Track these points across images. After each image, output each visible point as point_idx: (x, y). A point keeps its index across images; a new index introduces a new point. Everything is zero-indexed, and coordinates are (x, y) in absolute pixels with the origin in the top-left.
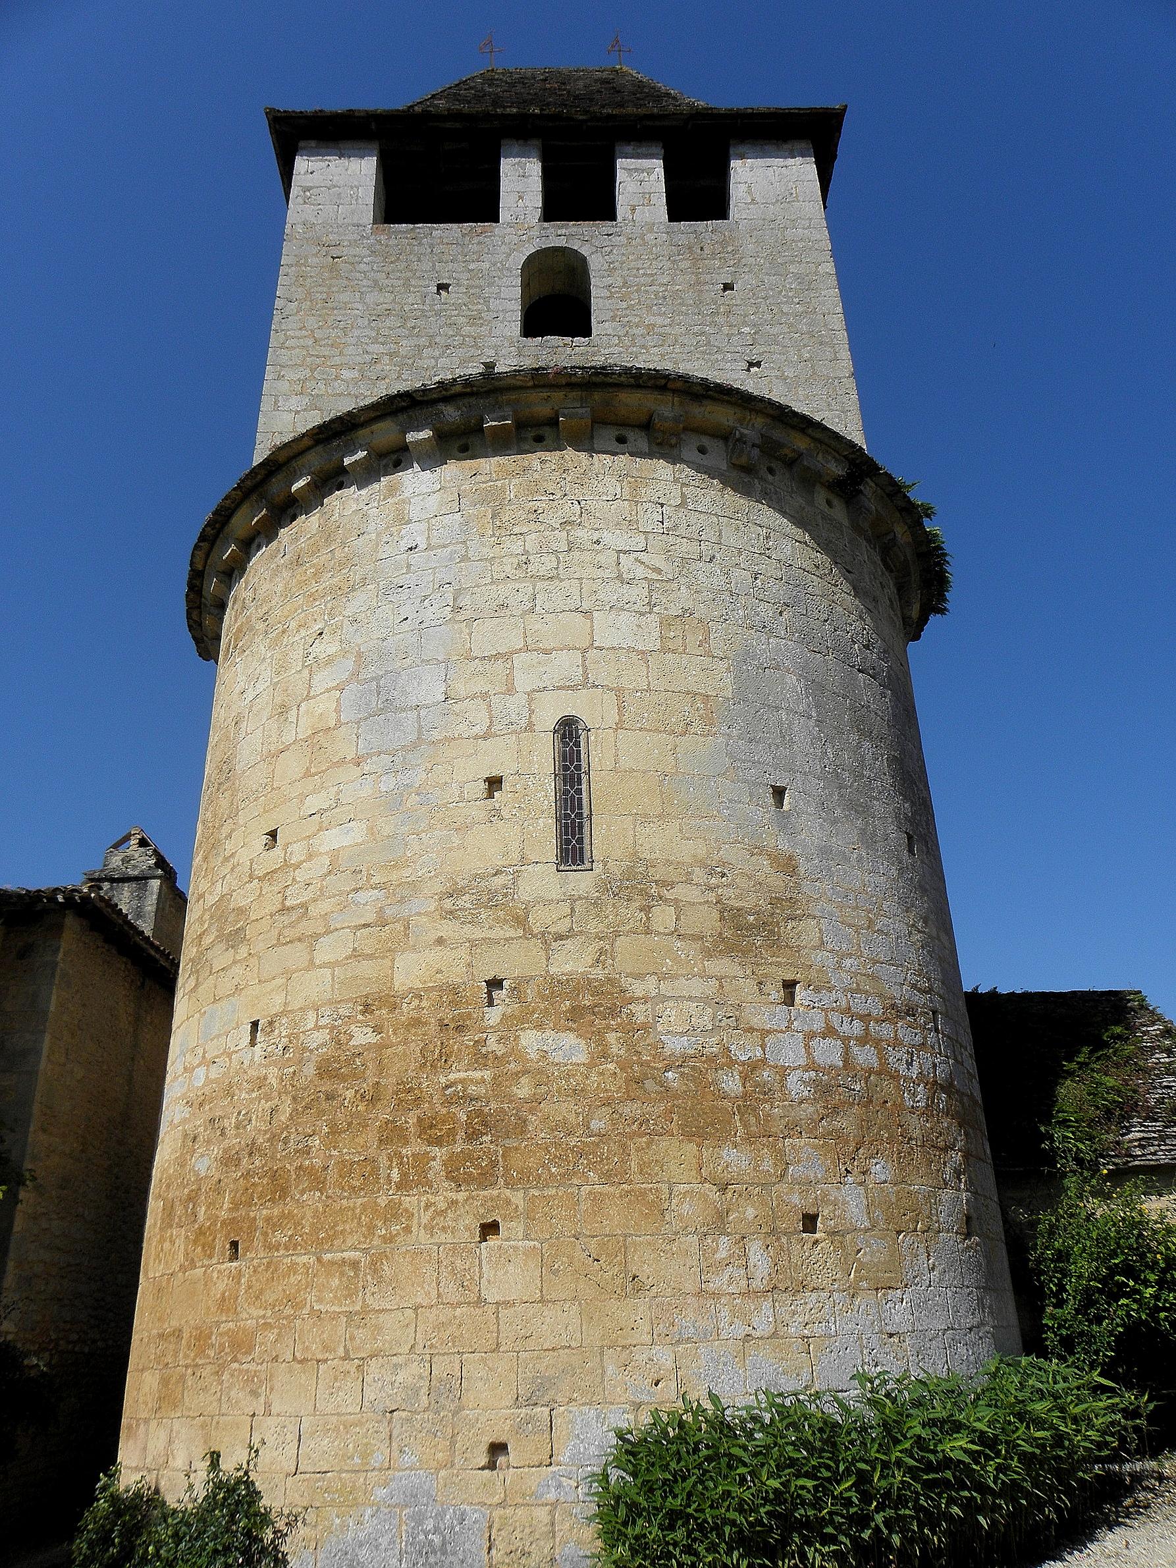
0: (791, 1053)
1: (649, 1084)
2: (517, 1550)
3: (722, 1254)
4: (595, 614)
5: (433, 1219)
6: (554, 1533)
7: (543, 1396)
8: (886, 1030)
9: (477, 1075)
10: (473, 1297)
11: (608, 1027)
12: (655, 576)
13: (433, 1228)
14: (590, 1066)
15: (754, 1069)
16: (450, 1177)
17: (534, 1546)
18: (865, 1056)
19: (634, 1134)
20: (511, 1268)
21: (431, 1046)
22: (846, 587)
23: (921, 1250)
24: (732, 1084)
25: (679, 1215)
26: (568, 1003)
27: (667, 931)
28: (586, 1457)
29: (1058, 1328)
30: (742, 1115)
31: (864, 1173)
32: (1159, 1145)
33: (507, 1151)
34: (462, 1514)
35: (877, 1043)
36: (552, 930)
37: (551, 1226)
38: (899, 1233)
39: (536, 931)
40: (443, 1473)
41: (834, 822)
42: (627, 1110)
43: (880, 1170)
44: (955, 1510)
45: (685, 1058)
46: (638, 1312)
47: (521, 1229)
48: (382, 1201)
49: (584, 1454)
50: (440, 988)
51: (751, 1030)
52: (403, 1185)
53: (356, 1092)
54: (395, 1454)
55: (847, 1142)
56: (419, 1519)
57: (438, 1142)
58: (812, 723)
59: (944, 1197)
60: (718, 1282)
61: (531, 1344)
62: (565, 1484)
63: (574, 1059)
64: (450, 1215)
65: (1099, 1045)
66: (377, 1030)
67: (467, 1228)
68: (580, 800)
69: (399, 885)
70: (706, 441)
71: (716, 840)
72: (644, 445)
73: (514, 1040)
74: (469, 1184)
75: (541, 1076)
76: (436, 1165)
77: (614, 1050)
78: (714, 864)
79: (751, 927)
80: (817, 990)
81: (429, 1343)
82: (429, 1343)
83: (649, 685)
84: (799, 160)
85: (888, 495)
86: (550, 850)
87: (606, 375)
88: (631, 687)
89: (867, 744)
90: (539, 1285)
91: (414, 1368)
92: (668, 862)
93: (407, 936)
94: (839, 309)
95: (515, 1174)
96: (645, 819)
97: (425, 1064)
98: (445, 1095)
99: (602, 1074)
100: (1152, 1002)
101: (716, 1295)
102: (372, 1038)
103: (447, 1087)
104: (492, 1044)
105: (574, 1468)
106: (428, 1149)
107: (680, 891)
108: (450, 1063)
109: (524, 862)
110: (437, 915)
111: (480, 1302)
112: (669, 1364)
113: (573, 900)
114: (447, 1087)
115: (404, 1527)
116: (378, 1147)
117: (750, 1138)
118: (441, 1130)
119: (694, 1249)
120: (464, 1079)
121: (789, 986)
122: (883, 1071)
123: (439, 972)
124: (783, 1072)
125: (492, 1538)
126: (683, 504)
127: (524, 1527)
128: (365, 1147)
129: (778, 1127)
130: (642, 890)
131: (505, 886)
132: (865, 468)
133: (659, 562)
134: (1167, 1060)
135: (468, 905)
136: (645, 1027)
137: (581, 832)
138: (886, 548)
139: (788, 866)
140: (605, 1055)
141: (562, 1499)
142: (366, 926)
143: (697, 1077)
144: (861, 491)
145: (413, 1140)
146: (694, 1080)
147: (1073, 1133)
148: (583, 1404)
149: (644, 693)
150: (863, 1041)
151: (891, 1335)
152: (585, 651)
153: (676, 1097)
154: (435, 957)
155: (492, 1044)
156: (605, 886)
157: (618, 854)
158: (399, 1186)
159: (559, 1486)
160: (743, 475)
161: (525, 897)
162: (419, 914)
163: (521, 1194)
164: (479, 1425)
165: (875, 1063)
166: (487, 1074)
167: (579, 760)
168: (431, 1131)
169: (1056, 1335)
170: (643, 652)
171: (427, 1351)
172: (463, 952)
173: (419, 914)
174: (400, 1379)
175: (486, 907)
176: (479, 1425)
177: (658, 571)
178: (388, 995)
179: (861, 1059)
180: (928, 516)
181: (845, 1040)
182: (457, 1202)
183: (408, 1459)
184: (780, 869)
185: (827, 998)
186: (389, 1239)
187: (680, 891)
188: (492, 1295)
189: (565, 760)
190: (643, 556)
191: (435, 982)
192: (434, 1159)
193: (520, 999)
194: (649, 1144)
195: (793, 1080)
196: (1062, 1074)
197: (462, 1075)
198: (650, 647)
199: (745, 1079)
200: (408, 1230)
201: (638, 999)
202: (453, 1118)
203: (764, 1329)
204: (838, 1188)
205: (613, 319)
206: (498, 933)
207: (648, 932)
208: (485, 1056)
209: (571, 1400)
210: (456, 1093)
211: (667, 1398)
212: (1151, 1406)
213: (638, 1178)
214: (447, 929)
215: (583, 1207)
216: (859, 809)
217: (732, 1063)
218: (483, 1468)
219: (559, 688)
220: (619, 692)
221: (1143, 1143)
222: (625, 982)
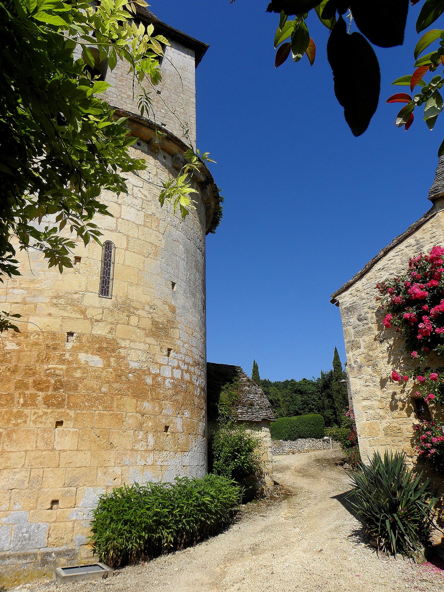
0: (167, 373)
1: (123, 378)
2: (59, 537)
3: (140, 437)
4: (123, 206)
5: (36, 418)
6: (74, 531)
7: (74, 483)
8: (192, 369)
9: (60, 367)
10: (51, 448)
11: (111, 356)
12: (144, 198)
13: (36, 422)
14: (103, 369)
15: (156, 376)
16: (45, 403)
17: (65, 536)
18: (187, 377)
19: (115, 395)
20: (67, 438)
21: (42, 354)
22: (198, 219)
23: (194, 440)
24: (149, 381)
25: (128, 423)
26: (98, 345)
27: (135, 325)
28: (88, 504)
29: (217, 468)
30: (151, 391)
31: (182, 414)
32: (246, 414)
33: (69, 396)
34: (39, 526)
35: (190, 373)
36: (95, 318)
37: (83, 424)
38: (189, 434)
39: (88, 317)
40: (32, 511)
41: (187, 298)
42: (114, 386)
43: (187, 414)
44: (203, 518)
45: (136, 370)
46: (111, 455)
47: (72, 424)
48: (15, 410)
49: (87, 503)
50: (48, 332)
51: (157, 363)
52: (25, 405)
53: (6, 367)
54: (12, 505)
55: (179, 404)
56: (20, 528)
57: (42, 390)
58: (185, 263)
59: (200, 424)
60: (138, 446)
61: (71, 465)
62: (79, 514)
63: (98, 366)
64: (44, 417)
65: (232, 382)
66: (18, 344)
67: (50, 423)
68: (109, 273)
69: (34, 290)
70: (166, 155)
71: (154, 297)
72: (146, 150)
73: (76, 356)
74: (53, 407)
75: (85, 369)
76: (40, 398)
77: (112, 364)
78: (152, 305)
79: (160, 329)
80: (177, 353)
81: (30, 464)
82: (30, 464)
83: (138, 237)
84: (190, 57)
85: (213, 191)
86: (97, 288)
87: (140, 119)
88: (132, 236)
89: (197, 274)
90: (77, 444)
91: (23, 473)
92: (138, 301)
93: (35, 310)
94: (195, 116)
95: (72, 404)
96: (131, 284)
97: (39, 360)
98: (46, 373)
99: (107, 372)
100: (244, 371)
101: (137, 451)
102: (16, 348)
103: (47, 370)
104: (67, 356)
105: (83, 508)
106: (37, 392)
107: (140, 312)
108: (49, 361)
109: (87, 291)
110: (49, 304)
111: (53, 450)
112: (120, 473)
113: (104, 308)
114: (47, 370)
115: (13, 532)
116: (15, 390)
117: (153, 400)
118: (43, 386)
119: (132, 435)
120: (55, 368)
121: (169, 350)
122: (191, 382)
123: (48, 326)
124: (165, 379)
125: (50, 534)
126: (156, 175)
127: (63, 529)
128: (9, 389)
129: (161, 397)
130: (128, 309)
131: (78, 299)
132: (210, 180)
133: (146, 193)
134: (249, 389)
135: (63, 303)
136: (124, 358)
137: (108, 284)
138: (207, 209)
139: (173, 310)
140: (109, 366)
141: (78, 519)
142: (16, 303)
143: (139, 377)
144: (206, 188)
145: (30, 388)
146: (138, 378)
147: (224, 408)
148: (89, 486)
149: (136, 239)
150: (187, 371)
151: (184, 466)
152: (117, 218)
153: (131, 383)
154: (47, 320)
155: (67, 356)
156: (115, 305)
157: (121, 295)
158: (23, 405)
159: (77, 514)
160: (176, 171)
161: (86, 304)
162: (42, 303)
163: (73, 412)
164: (48, 494)
165: (189, 379)
166: (64, 367)
167: (111, 258)
168: (38, 385)
169: (216, 470)
170: (138, 225)
171: (29, 467)
172: (59, 320)
173: (42, 303)
174: (16, 477)
175: (70, 305)
176: (48, 494)
177: (146, 196)
178: (24, 332)
179: (185, 377)
180: (222, 201)
181: (182, 370)
182: (47, 413)
183: (17, 507)
184: (171, 311)
185: (179, 356)
186: (17, 425)
187: (140, 312)
188: (58, 447)
189: (105, 256)
190: (141, 189)
191: (46, 330)
192: (39, 396)
193: (80, 341)
194: (121, 398)
195: (167, 381)
196: (220, 390)
197: (54, 366)
198: (139, 223)
199: (153, 379)
200: (25, 422)
201: (122, 347)
202: (49, 382)
203: (150, 462)
204: (176, 418)
205: (116, 87)
206: (73, 315)
207: (128, 324)
208: (64, 360)
209: (84, 485)
210: (51, 373)
211: (118, 483)
212: (245, 490)
213: (116, 409)
214: (53, 310)
215: (96, 418)
216: (194, 295)
217: (150, 374)
218: (48, 509)
219: (107, 229)
220: (128, 236)
221: (242, 413)
222: (119, 341)
